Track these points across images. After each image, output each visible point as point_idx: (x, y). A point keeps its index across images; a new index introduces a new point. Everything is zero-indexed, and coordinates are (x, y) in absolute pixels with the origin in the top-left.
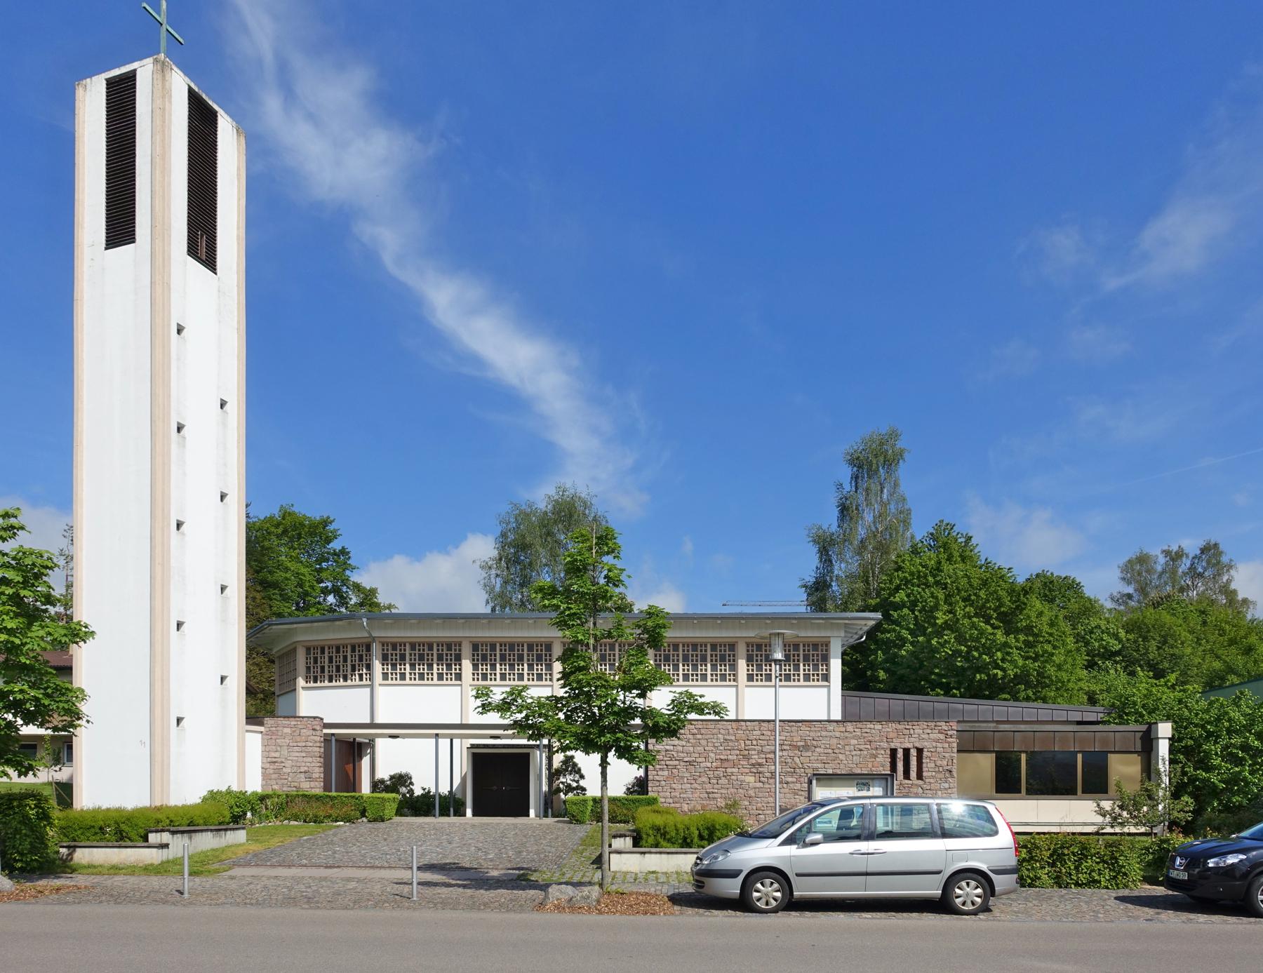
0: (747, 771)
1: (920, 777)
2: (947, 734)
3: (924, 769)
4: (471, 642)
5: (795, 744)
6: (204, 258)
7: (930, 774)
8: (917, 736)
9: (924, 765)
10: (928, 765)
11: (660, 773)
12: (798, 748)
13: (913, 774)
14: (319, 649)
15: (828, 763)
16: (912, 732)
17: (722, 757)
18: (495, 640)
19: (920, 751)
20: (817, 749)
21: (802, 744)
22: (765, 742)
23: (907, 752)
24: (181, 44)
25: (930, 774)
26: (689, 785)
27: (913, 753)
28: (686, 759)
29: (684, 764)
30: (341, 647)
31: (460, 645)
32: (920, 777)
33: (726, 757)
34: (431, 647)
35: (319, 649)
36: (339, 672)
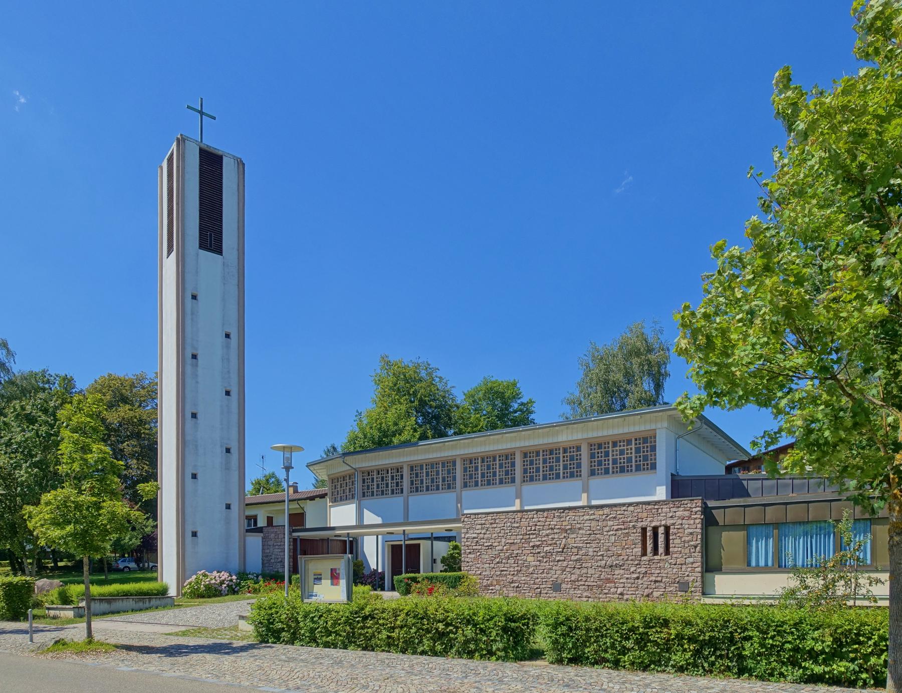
0: (528, 552)
1: (667, 552)
2: (692, 511)
3: (671, 545)
4: (521, 451)
5: (563, 527)
6: (743, 481)
7: (676, 549)
8: (664, 514)
9: (671, 541)
10: (675, 542)
11: (469, 556)
12: (566, 531)
13: (661, 550)
14: (479, 459)
15: (590, 543)
16: (660, 511)
17: (510, 541)
18: (538, 447)
19: (667, 529)
20: (581, 532)
21: (569, 527)
22: (541, 527)
23: (655, 530)
24: (202, 99)
25: (676, 549)
26: (488, 565)
27: (661, 530)
28: (486, 544)
29: (485, 548)
30: (541, 452)
31: (514, 455)
32: (667, 552)
33: (512, 541)
34: (538, 454)
35: (479, 459)
36: (436, 471)
